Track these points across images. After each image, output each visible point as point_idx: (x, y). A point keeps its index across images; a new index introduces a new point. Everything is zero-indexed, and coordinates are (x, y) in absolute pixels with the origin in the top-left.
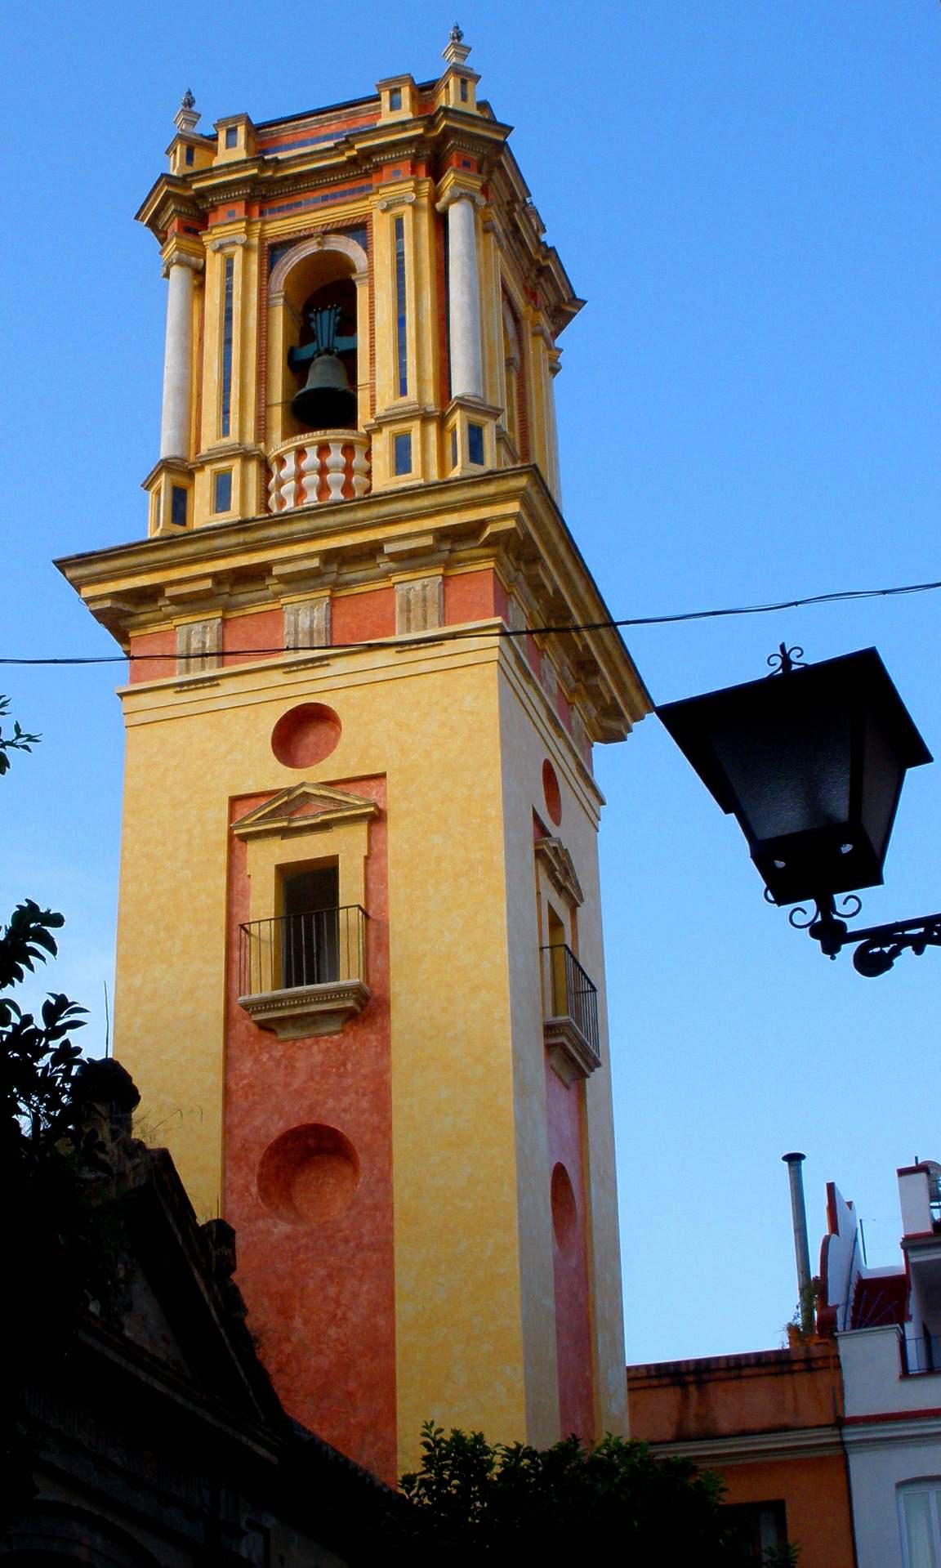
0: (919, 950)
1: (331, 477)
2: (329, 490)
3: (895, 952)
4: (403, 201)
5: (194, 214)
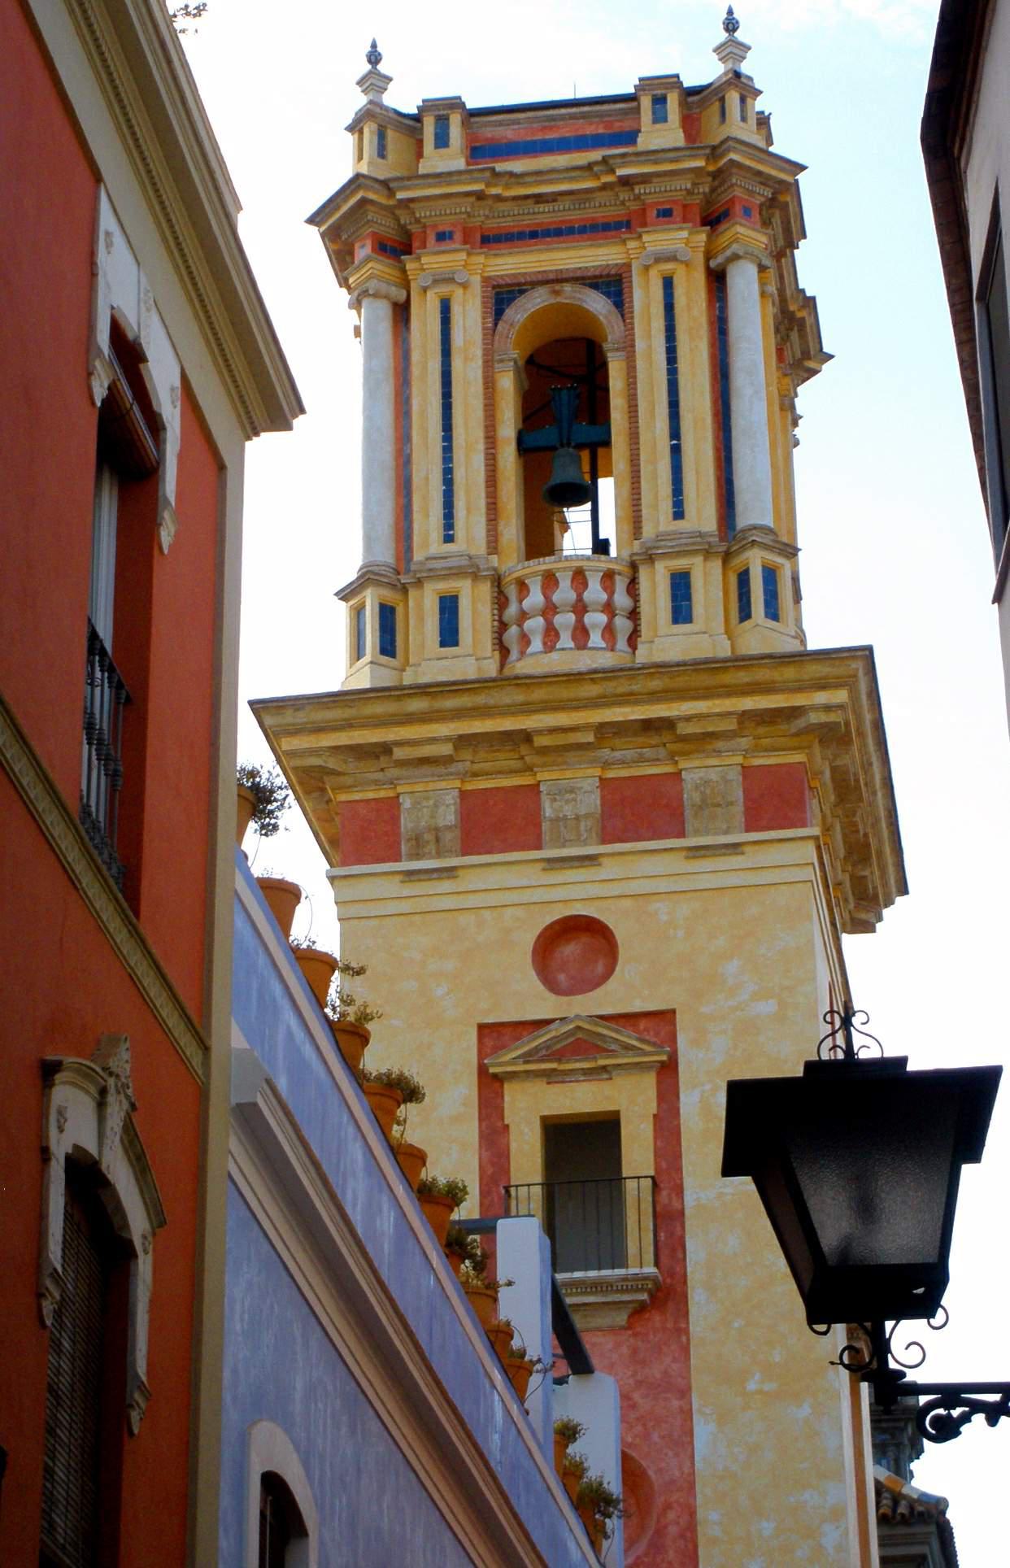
0: (992, 1421)
1: (588, 619)
2: (557, 635)
3: (965, 1418)
4: (453, 279)
5: (392, 226)
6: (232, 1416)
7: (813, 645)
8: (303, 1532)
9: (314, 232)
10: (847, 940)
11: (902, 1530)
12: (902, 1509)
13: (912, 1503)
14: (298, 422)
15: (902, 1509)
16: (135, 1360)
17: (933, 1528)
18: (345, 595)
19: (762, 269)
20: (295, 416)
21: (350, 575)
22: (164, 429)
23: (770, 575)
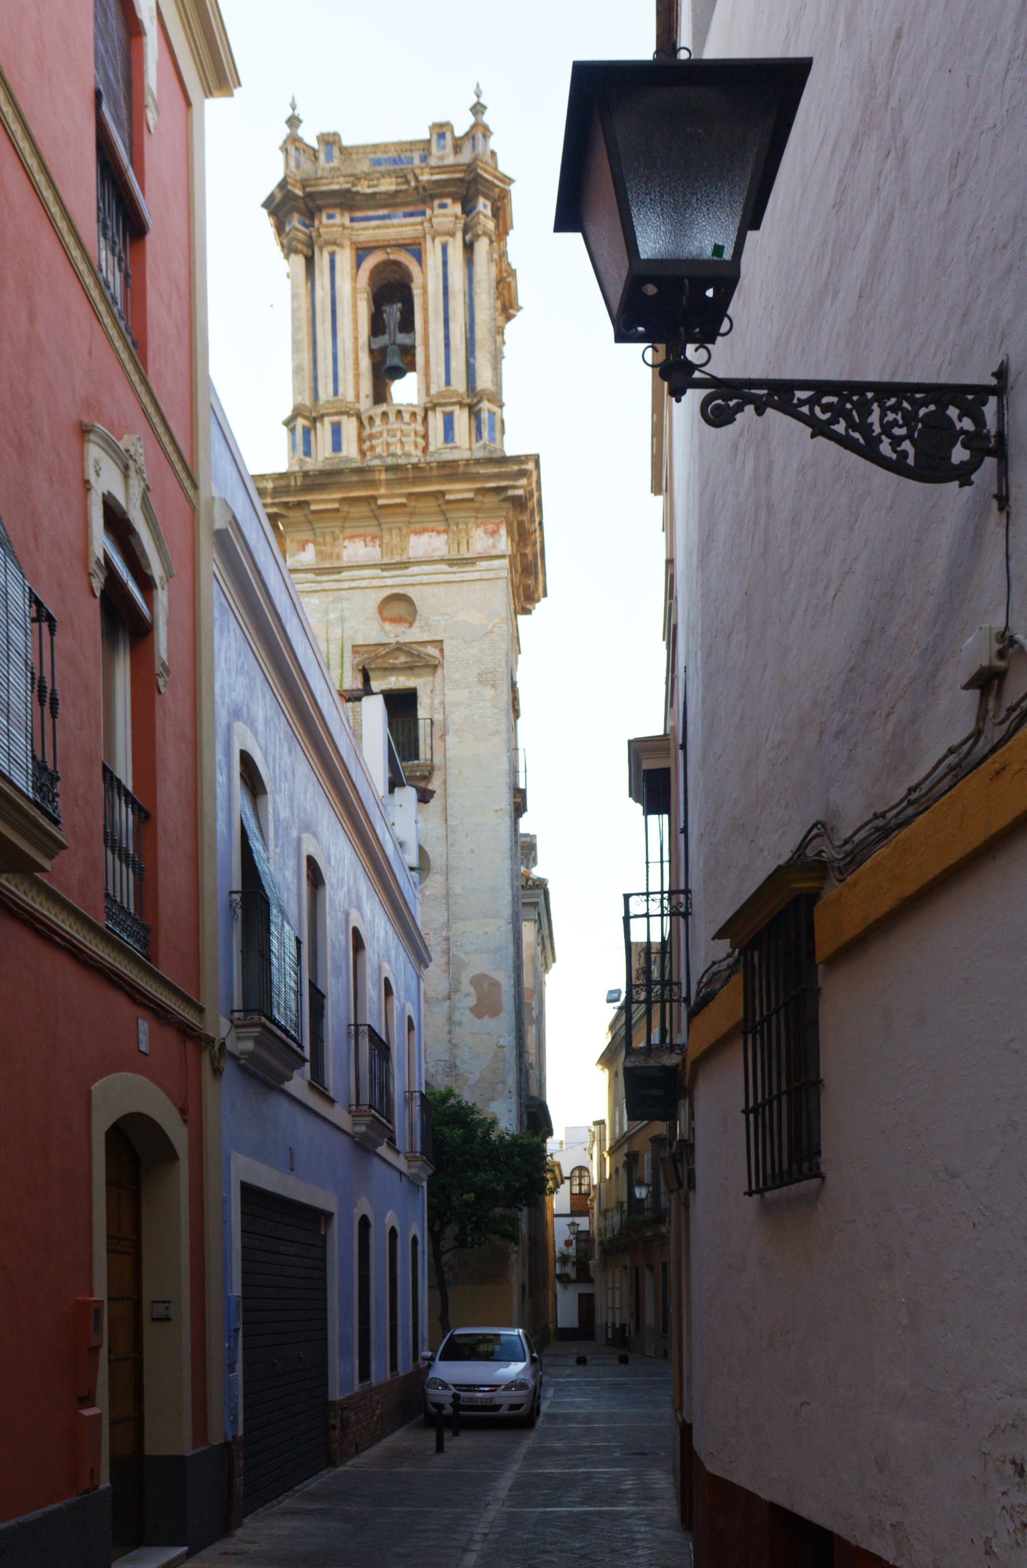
3: (739, 408)
6: (222, 716)
7: (510, 451)
8: (265, 792)
9: (285, 429)
10: (519, 617)
11: (529, 892)
12: (530, 883)
13: (534, 881)
14: (237, 92)
15: (530, 883)
16: (159, 650)
17: (542, 891)
18: (286, 423)
19: (491, 242)
20: (235, 87)
21: (288, 412)
22: (145, 34)
23: (492, 414)
